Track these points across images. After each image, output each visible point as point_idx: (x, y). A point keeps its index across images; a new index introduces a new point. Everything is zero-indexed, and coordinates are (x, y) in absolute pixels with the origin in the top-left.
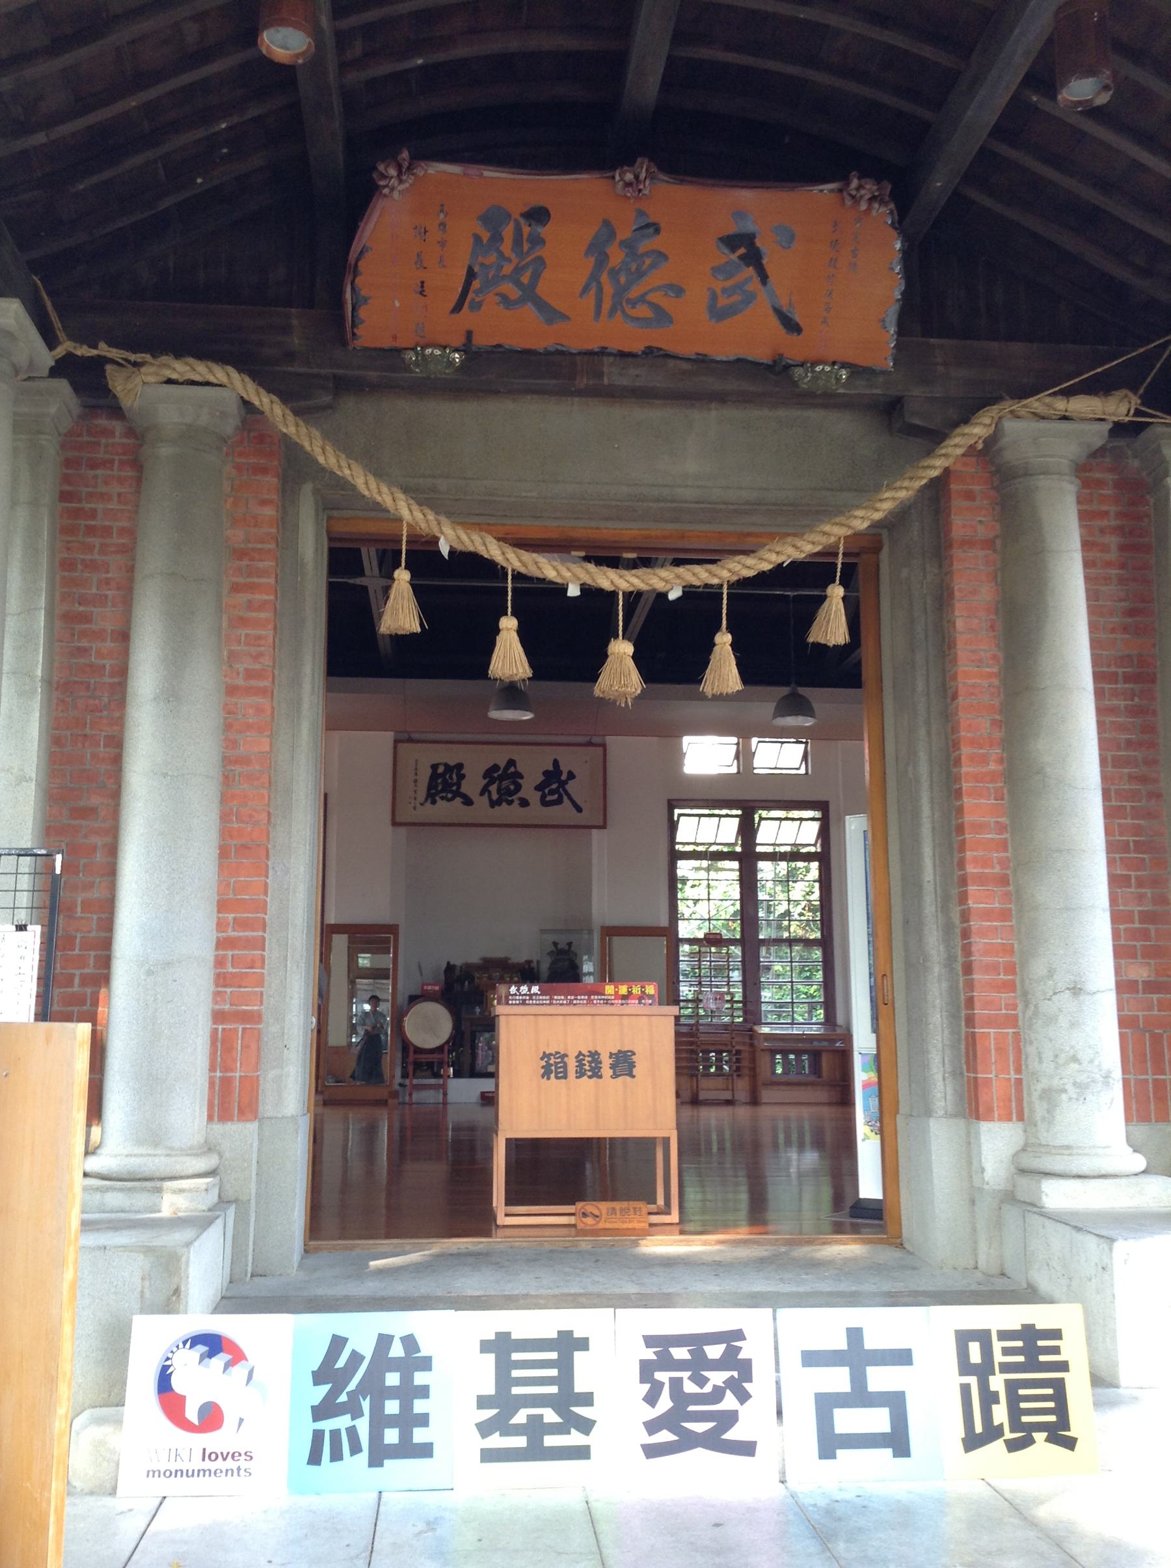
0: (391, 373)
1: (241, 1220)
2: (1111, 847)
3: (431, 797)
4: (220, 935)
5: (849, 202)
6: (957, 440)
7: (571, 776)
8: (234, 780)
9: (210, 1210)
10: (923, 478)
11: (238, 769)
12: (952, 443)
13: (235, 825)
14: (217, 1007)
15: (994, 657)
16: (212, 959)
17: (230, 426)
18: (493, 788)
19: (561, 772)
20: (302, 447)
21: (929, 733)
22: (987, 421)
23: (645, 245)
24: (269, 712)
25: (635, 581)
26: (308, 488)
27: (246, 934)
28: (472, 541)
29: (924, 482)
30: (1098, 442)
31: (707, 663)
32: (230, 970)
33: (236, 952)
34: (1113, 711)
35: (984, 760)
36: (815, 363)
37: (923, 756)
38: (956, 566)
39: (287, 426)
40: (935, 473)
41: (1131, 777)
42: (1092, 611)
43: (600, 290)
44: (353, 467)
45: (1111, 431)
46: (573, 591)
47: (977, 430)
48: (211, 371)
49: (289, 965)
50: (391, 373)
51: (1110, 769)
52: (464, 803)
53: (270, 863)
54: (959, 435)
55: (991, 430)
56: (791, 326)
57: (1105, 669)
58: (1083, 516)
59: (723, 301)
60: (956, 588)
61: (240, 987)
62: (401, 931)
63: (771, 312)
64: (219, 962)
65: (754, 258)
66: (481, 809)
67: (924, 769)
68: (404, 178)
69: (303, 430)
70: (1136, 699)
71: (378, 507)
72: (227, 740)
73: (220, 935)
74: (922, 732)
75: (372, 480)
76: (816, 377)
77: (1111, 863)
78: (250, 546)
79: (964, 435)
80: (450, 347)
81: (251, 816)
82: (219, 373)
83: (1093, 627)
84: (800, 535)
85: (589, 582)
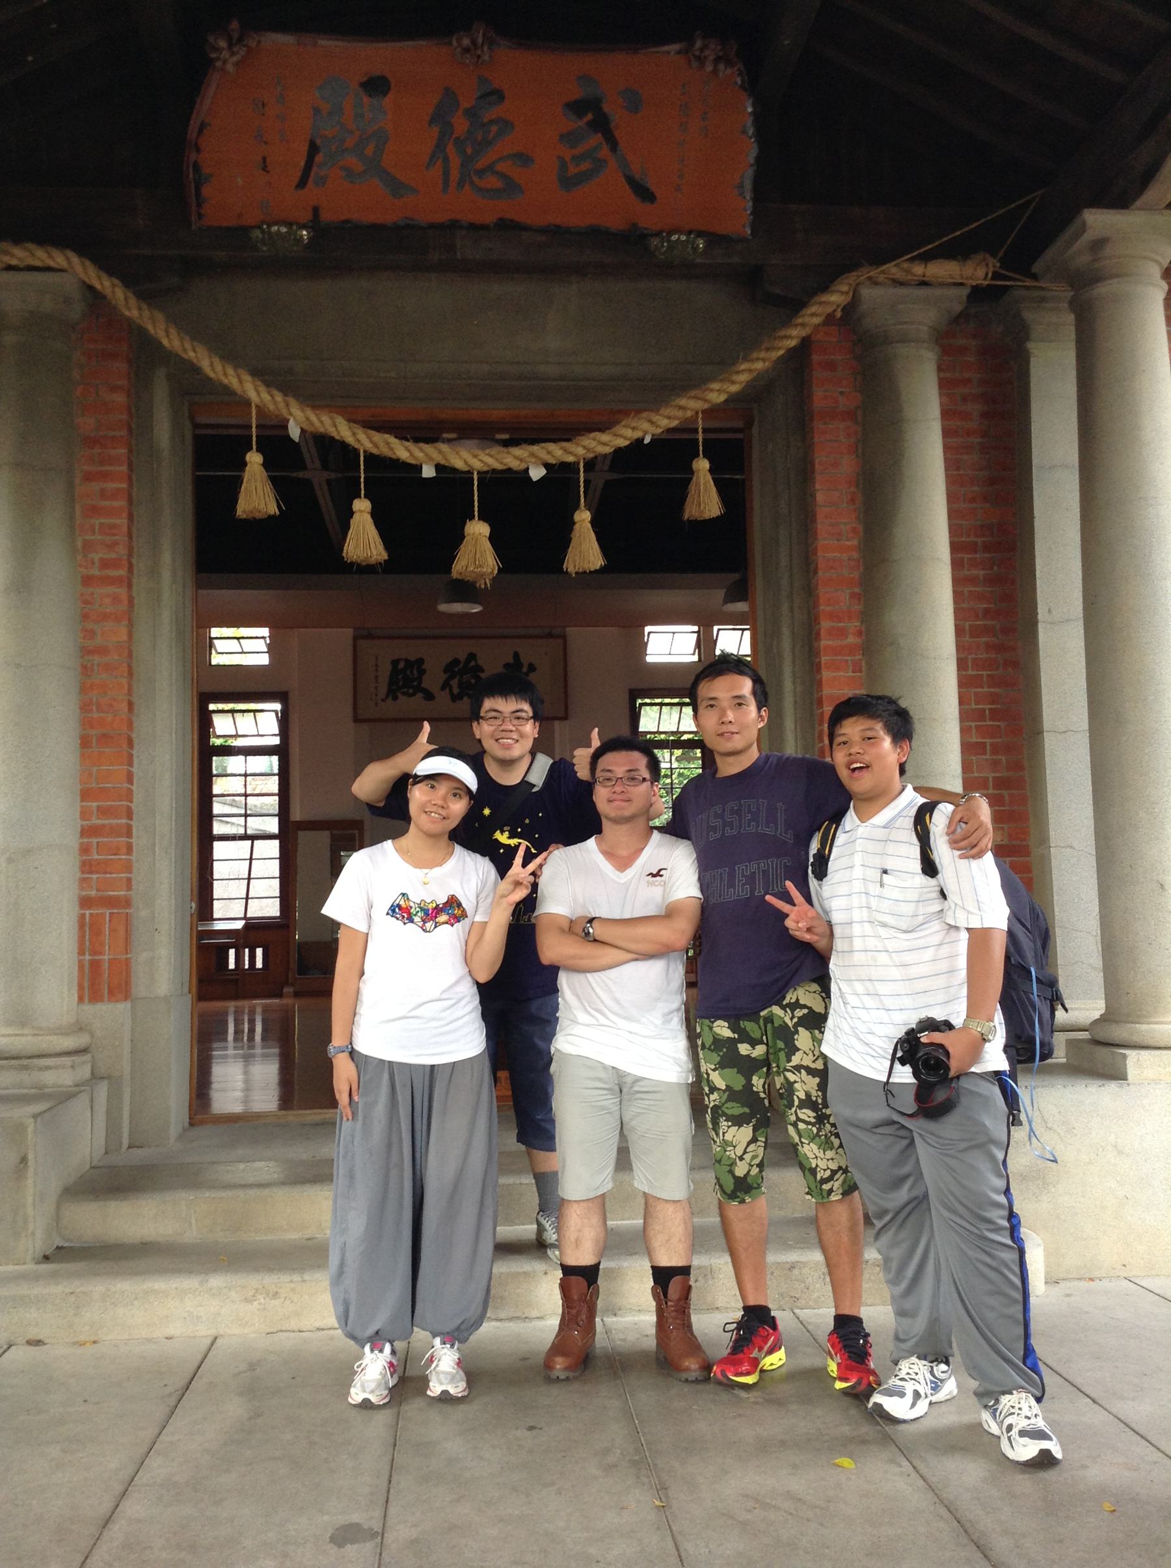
0: (237, 253)
1: (115, 1096)
2: (964, 716)
3: (392, 693)
5: (695, 64)
6: (814, 309)
7: (532, 668)
8: (92, 671)
10: (779, 348)
11: (97, 659)
12: (809, 312)
13: (95, 715)
14: (84, 893)
15: (854, 530)
16: (76, 846)
17: (76, 312)
18: (454, 683)
19: (521, 665)
20: (147, 330)
21: (791, 609)
22: (845, 288)
24: (126, 602)
25: (490, 461)
26: (161, 374)
28: (322, 422)
29: (781, 352)
30: (958, 308)
32: (96, 857)
33: (100, 840)
34: (972, 580)
35: (842, 633)
36: (670, 234)
37: (786, 632)
38: (816, 440)
40: (792, 343)
41: (989, 647)
43: (446, 159)
44: (198, 349)
46: (428, 472)
47: (835, 299)
48: (50, 256)
50: (237, 253)
51: (967, 638)
53: (134, 752)
54: (816, 303)
55: (849, 298)
56: (645, 194)
58: (943, 384)
59: (573, 170)
61: (106, 873)
64: (85, 850)
65: (601, 125)
67: (786, 644)
68: (235, 49)
69: (146, 313)
70: (996, 568)
71: (227, 391)
72: (84, 630)
74: (785, 608)
75: (217, 361)
76: (672, 246)
77: (964, 731)
79: (821, 303)
80: (298, 224)
81: (111, 705)
82: (59, 258)
83: (951, 498)
84: (657, 411)
85: (443, 462)
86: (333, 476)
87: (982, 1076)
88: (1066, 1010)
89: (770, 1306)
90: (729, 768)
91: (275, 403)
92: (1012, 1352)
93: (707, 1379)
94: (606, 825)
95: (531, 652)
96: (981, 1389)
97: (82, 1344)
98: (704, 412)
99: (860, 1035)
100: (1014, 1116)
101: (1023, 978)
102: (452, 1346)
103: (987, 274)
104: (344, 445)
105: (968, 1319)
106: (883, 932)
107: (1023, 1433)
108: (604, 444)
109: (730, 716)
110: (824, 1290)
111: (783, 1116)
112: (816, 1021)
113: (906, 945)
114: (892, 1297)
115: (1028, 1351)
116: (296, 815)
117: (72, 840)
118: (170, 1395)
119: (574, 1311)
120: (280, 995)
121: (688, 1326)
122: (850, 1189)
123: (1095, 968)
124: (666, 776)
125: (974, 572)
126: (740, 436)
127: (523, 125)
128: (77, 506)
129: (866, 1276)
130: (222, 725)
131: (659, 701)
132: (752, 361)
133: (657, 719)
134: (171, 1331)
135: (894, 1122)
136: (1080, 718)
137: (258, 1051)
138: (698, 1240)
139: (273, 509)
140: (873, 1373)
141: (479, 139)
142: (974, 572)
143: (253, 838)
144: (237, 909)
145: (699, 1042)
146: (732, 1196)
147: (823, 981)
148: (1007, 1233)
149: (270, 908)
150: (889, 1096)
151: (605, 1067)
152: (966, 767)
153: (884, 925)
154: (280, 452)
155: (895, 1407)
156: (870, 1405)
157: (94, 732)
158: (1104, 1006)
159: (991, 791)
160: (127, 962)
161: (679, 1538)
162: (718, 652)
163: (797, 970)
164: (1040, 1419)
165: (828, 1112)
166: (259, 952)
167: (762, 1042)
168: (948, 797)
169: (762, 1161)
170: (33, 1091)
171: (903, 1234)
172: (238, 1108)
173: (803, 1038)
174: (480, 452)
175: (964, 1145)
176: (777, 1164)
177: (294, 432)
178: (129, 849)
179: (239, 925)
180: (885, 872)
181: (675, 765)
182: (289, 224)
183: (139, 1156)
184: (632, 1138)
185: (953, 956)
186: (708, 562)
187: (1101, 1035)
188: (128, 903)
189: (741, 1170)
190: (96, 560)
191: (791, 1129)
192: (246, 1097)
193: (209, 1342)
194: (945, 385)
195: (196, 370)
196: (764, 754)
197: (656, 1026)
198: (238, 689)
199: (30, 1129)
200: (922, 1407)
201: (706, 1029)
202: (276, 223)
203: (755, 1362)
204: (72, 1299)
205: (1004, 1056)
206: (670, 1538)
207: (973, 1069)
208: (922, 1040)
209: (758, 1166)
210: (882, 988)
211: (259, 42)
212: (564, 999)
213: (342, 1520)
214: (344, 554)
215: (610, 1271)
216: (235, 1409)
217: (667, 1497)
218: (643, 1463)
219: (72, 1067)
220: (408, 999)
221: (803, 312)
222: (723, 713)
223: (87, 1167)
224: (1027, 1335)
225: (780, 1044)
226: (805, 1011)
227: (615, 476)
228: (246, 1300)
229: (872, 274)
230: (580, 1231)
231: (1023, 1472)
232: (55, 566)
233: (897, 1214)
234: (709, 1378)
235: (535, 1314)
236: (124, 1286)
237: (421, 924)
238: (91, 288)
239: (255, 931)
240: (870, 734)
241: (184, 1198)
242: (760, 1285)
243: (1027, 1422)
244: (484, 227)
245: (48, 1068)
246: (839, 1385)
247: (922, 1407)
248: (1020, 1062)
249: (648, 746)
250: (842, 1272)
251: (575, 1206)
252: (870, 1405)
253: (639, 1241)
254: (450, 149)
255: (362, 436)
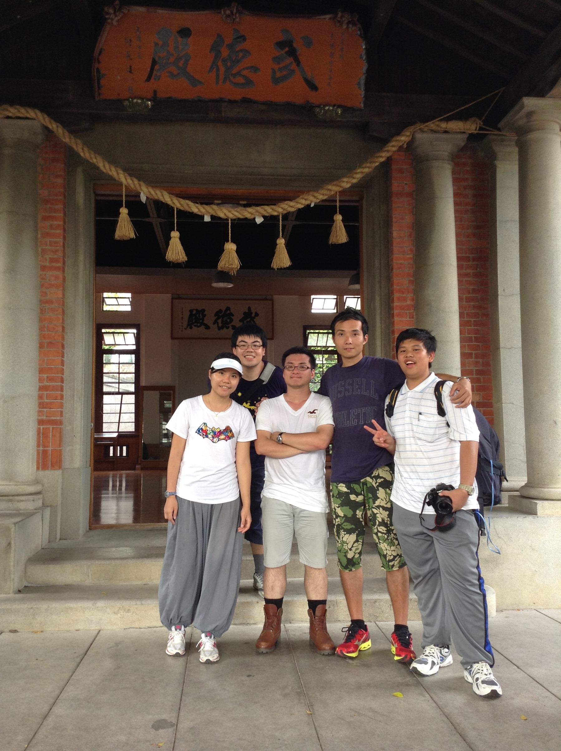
2: (462, 340)
4: (41, 384)
5: (338, 24)
6: (393, 143)
7: (257, 314)
8: (45, 312)
9: (35, 509)
10: (377, 162)
11: (47, 306)
14: (40, 418)
16: (37, 395)
18: (220, 321)
19: (252, 313)
21: (380, 287)
23: (238, 47)
26: (80, 170)
27: (53, 384)
28: (156, 194)
29: (377, 164)
30: (463, 144)
31: (274, 253)
32: (46, 401)
33: (48, 392)
34: (467, 275)
35: (405, 299)
36: (325, 106)
37: (377, 298)
39: (65, 138)
40: (382, 160)
41: (474, 307)
42: (457, 227)
43: (218, 70)
44: (98, 158)
45: (468, 139)
46: (207, 219)
47: (404, 138)
48: (27, 112)
49: (75, 399)
52: (206, 328)
56: (313, 87)
57: (464, 255)
59: (278, 75)
60: (394, 216)
62: (177, 389)
63: (302, 80)
64: (40, 397)
65: (292, 53)
66: (214, 331)
67: (378, 304)
68: (117, 14)
69: (73, 140)
70: (478, 269)
71: (111, 178)
73: (41, 384)
74: (377, 287)
76: (326, 112)
77: (462, 347)
78: (51, 198)
79: (397, 141)
81: (54, 329)
82: (31, 113)
83: (458, 235)
84: (317, 191)
85: (214, 214)
86: (163, 220)
87: (466, 511)
88: (507, 481)
89: (364, 620)
90: (347, 364)
91: (134, 184)
92: (479, 643)
93: (334, 654)
94: (289, 389)
95: (256, 307)
96: (464, 661)
97: (36, 632)
98: (340, 192)
99: (409, 492)
100: (482, 531)
101: (487, 465)
102: (211, 637)
103: (476, 128)
104: (167, 205)
105: (458, 628)
106: (419, 442)
107: (483, 682)
108: (292, 207)
109: (350, 340)
110: (389, 612)
111: (371, 530)
112: (388, 485)
113: (431, 448)
114: (422, 617)
115: (487, 644)
116: (143, 383)
117: (35, 393)
118: (77, 657)
119: (270, 621)
120: (134, 469)
121: (326, 628)
122: (402, 565)
123: (523, 462)
124: (320, 367)
125: (468, 271)
126: (357, 204)
127: (255, 53)
128: (39, 232)
129: (410, 606)
130: (108, 339)
131: (317, 331)
132: (363, 168)
133: (315, 340)
134: (79, 627)
135: (423, 533)
136: (517, 342)
137: (124, 495)
138: (330, 588)
139: (132, 235)
140: (413, 652)
141: (234, 59)
142: (468, 271)
143: (122, 394)
144: (114, 428)
145: (331, 494)
146: (346, 568)
147: (391, 466)
148: (478, 587)
149: (130, 427)
150: (422, 520)
151: (286, 504)
152: (463, 364)
153: (420, 439)
154: (137, 209)
155: (423, 669)
156: (411, 668)
157: (46, 341)
158: (527, 479)
159: (474, 376)
160: (61, 451)
161: (318, 729)
162: (346, 307)
163: (379, 460)
164: (492, 675)
165: (392, 528)
166: (124, 448)
167: (361, 494)
168: (452, 378)
169: (361, 551)
170: (15, 512)
171: (428, 587)
172: (113, 522)
173: (381, 493)
174: (232, 210)
175: (457, 544)
176: (369, 553)
177: (143, 199)
178: (62, 397)
179: (115, 435)
180: (420, 414)
181: (325, 362)
182: (142, 99)
183: (65, 543)
184: (299, 539)
185: (453, 454)
186: (340, 264)
187: (525, 493)
188: (61, 423)
189: (350, 555)
190: (48, 258)
191: (375, 536)
192: (117, 516)
193: (96, 632)
194: (455, 181)
195: (96, 168)
196: (365, 356)
197: (311, 485)
198: (117, 322)
199: (13, 530)
200: (436, 669)
201: (335, 487)
202: (135, 98)
203: (357, 647)
204: (32, 610)
205: (477, 502)
206: (314, 729)
207: (463, 509)
208: (439, 494)
209: (359, 553)
210: (419, 469)
211: (129, 10)
212: (268, 471)
213: (157, 717)
214: (166, 258)
215: (288, 602)
216: (108, 664)
217: (313, 710)
218: (302, 693)
219: (33, 500)
220: (203, 474)
221: (388, 145)
222: (347, 339)
223: (40, 548)
224: (486, 636)
225: (370, 495)
226: (382, 480)
227: (298, 223)
228: (114, 613)
229: (421, 127)
230: (273, 582)
231: (483, 700)
232: (28, 261)
233: (425, 577)
234: (335, 654)
235: (252, 622)
236: (56, 605)
237: (211, 439)
238: (47, 128)
239: (123, 438)
240: (416, 348)
241: (85, 564)
242: (360, 611)
243: (486, 677)
244: (235, 102)
245: (22, 501)
246: (396, 658)
247: (436, 669)
248: (485, 505)
249: (311, 353)
250: (398, 605)
251: (272, 570)
252: (411, 668)
253: (302, 588)
254: (220, 64)
255: (175, 201)
